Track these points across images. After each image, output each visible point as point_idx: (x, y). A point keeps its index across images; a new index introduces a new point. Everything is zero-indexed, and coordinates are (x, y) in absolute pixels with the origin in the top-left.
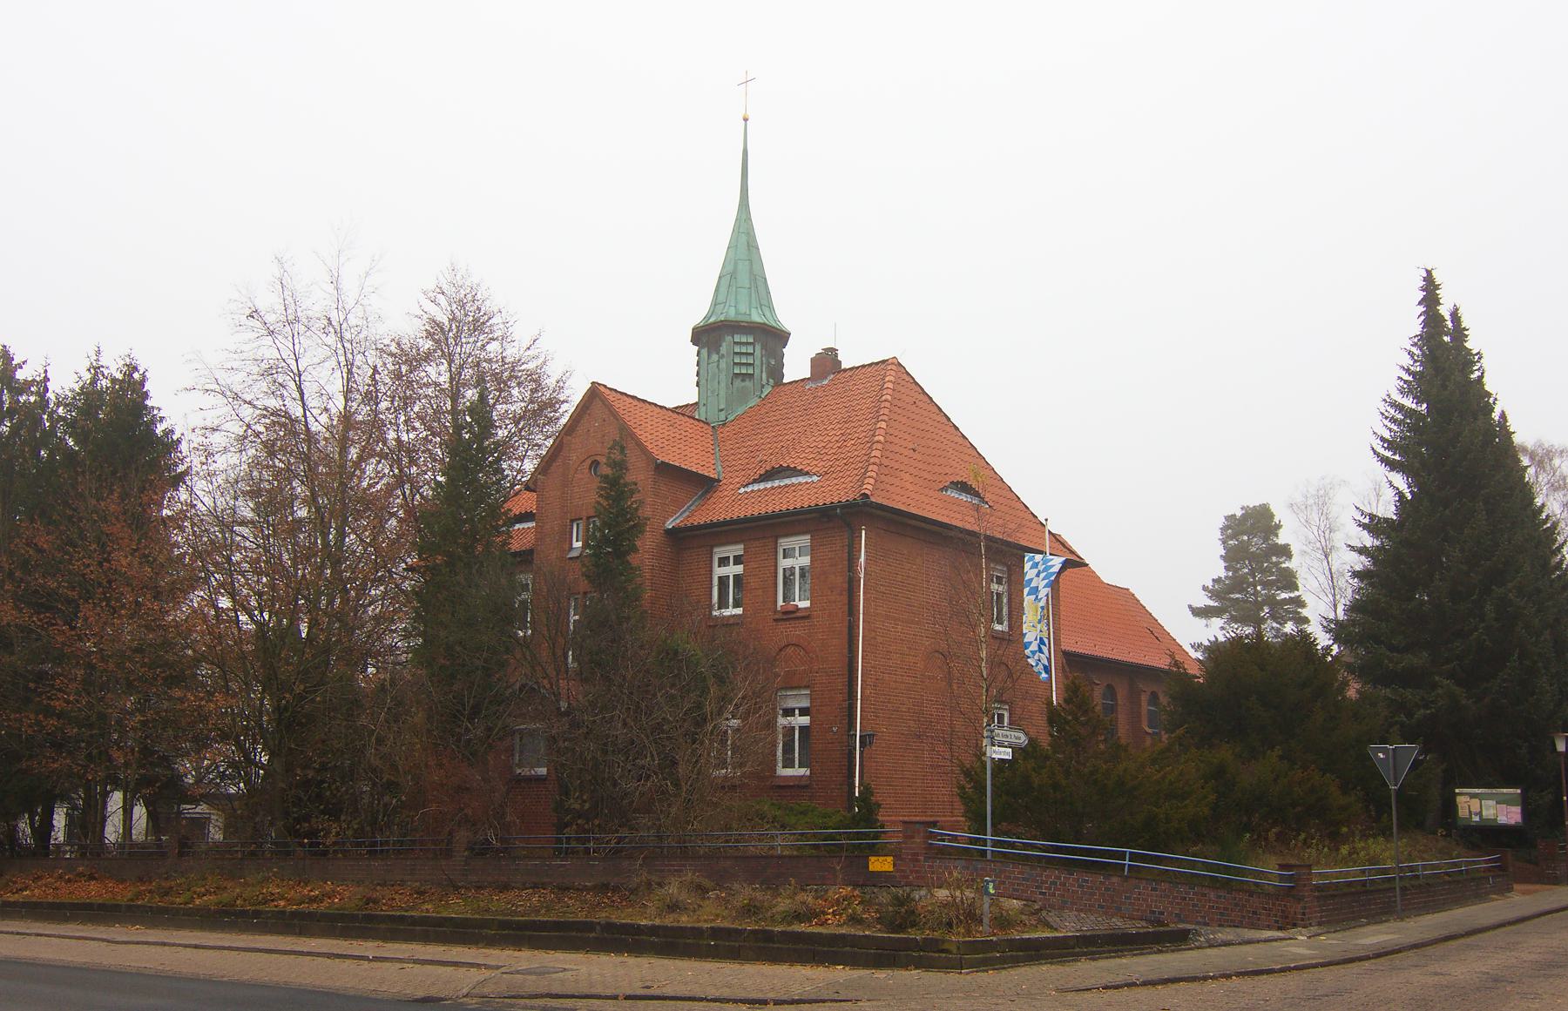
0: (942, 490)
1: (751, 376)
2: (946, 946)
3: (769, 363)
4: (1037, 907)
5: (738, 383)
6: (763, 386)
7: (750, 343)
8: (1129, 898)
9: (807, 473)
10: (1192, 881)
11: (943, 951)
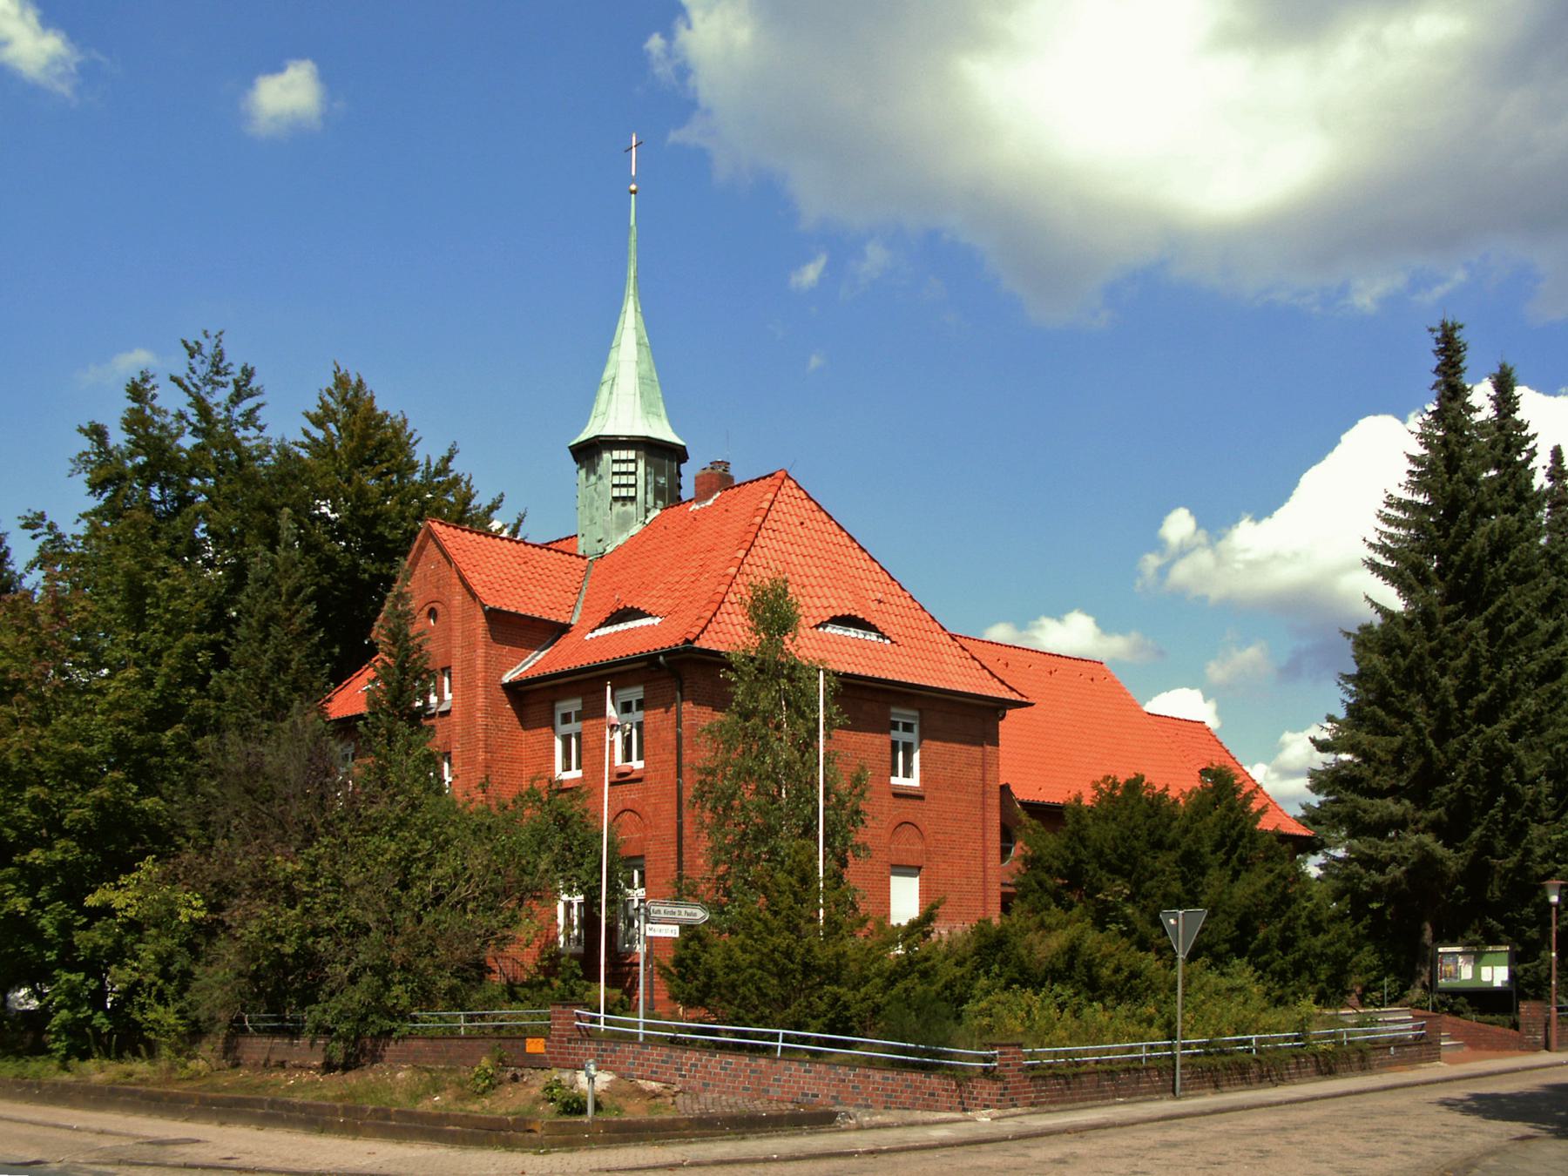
0: (817, 627)
1: (633, 499)
2: (531, 1127)
3: (656, 482)
4: (676, 1089)
5: (618, 506)
6: (647, 510)
7: (631, 461)
8: (779, 1080)
9: (650, 615)
10: (871, 1063)
11: (530, 1131)
